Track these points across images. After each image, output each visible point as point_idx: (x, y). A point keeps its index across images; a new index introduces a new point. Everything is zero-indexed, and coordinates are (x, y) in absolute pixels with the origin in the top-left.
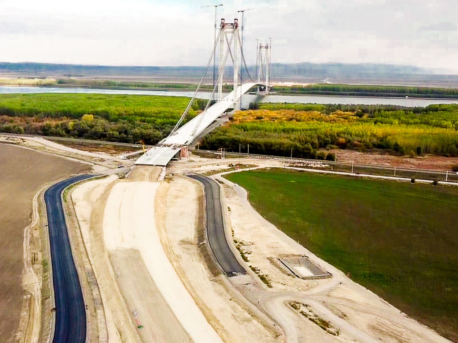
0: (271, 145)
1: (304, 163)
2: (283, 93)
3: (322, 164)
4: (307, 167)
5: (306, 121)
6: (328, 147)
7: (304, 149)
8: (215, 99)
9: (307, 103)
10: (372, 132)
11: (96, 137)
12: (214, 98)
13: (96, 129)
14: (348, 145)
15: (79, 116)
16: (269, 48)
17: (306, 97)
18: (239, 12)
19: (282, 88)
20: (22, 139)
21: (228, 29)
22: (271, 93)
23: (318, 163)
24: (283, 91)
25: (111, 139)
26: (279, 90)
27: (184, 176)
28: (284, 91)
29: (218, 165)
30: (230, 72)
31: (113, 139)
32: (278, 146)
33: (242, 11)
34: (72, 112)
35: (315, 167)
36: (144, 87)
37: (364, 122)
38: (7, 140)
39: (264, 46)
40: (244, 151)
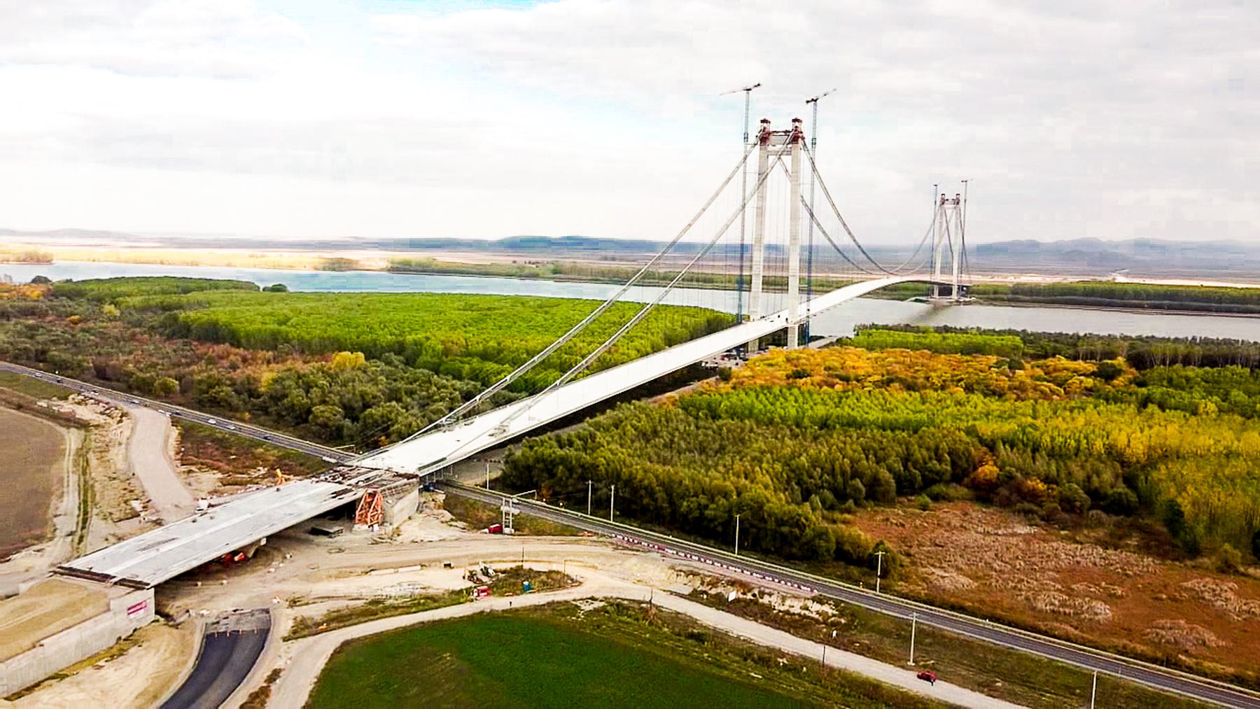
3: (814, 599)
4: (751, 609)
6: (1011, 461)
8: (744, 312)
10: (1111, 441)
16: (962, 202)
18: (808, 102)
19: (992, 290)
21: (776, 145)
26: (984, 293)
28: (996, 296)
32: (703, 500)
33: (813, 100)
37: (1107, 400)
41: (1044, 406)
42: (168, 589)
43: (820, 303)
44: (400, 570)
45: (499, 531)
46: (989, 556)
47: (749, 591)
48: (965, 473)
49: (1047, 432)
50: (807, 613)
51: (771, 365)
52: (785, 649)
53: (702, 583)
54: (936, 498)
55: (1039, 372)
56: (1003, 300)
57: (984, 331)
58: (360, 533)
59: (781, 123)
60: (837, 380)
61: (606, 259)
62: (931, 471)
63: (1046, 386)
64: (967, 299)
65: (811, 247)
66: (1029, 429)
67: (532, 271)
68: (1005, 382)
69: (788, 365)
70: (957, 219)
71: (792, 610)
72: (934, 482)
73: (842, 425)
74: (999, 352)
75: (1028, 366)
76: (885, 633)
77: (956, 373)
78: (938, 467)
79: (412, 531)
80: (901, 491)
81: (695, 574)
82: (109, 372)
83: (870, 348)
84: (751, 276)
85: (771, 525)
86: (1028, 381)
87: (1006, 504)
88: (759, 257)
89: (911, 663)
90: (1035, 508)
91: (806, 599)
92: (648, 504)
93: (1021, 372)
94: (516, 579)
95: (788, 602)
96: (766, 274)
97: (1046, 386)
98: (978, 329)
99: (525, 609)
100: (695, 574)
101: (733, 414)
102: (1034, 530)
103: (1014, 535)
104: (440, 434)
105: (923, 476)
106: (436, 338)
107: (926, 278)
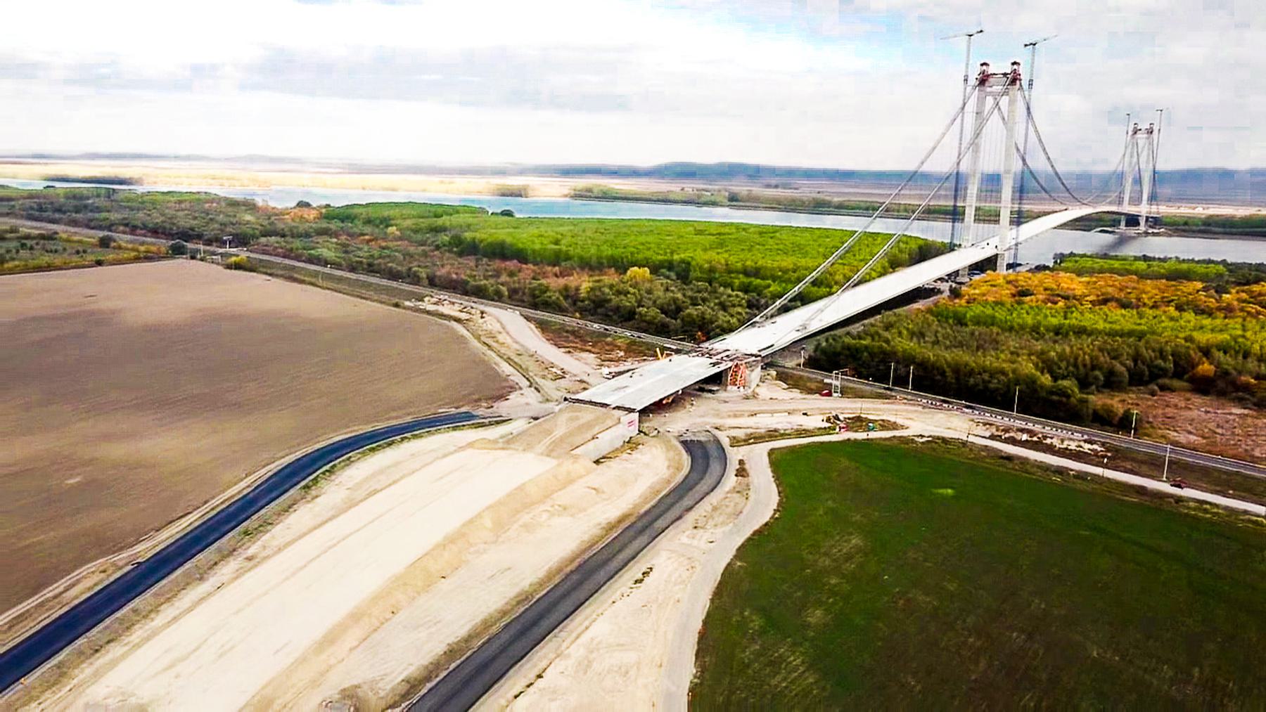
2: (1184, 231)
3: (1085, 441)
7: (1052, 393)
9: (1201, 258)
11: (619, 317)
14: (1221, 384)
16: (1156, 132)
17: (1240, 242)
18: (1026, 45)
20: (482, 313)
21: (996, 87)
22: (1150, 231)
24: (1183, 228)
30: (992, 182)
36: (868, 210)
38: (461, 311)
39: (1143, 129)
41: (1252, 323)
43: (1029, 229)
44: (775, 415)
45: (829, 394)
46: (1212, 426)
47: (1035, 435)
48: (1185, 371)
49: (1257, 341)
50: (1081, 449)
51: (994, 286)
52: (1072, 467)
53: (997, 430)
54: (1163, 388)
55: (1244, 296)
56: (1194, 232)
57: (1184, 260)
58: (732, 392)
59: (1000, 66)
60: (1060, 299)
61: (768, 186)
62: (1156, 366)
63: (1252, 308)
64: (1156, 231)
65: (958, 173)
66: (1240, 340)
67: (708, 199)
68: (1212, 303)
69: (1009, 286)
70: (1149, 149)
71: (1069, 447)
72: (1159, 377)
73: (1074, 333)
74: (1204, 278)
75: (1234, 291)
76: (1143, 462)
77: (1166, 295)
78: (1163, 364)
79: (764, 391)
80: (1131, 384)
81: (991, 425)
83: (1079, 274)
84: (964, 207)
85: (1044, 394)
86: (1235, 303)
87: (1222, 394)
88: (973, 189)
89: (1164, 479)
90: (1247, 396)
91: (1080, 441)
92: (939, 381)
93: (1228, 296)
94: (858, 422)
95: (1066, 443)
97: (1252, 308)
98: (1177, 258)
99: (876, 439)
100: (991, 425)
101: (978, 321)
102: (1246, 412)
103: (1231, 414)
104: (756, 329)
105: (1150, 371)
106: (701, 257)
107: (1114, 208)
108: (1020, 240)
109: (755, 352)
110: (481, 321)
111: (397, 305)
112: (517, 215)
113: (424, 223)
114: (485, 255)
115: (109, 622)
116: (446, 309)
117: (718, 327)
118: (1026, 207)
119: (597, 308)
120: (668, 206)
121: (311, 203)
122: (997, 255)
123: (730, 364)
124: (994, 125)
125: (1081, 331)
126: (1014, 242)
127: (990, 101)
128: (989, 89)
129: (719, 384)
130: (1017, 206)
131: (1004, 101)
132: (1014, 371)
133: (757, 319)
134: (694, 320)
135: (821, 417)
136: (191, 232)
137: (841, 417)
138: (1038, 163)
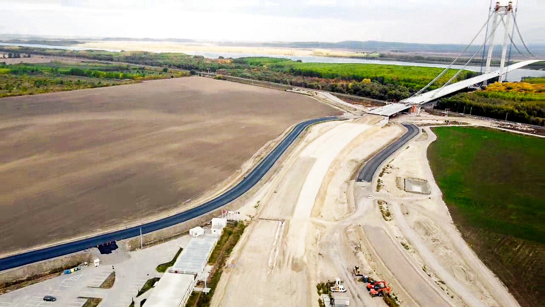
0: (491, 109)
1: (511, 126)
3: (529, 128)
4: (514, 129)
5: (138, 70)
8: (483, 72)
12: (481, 71)
13: (366, 89)
15: (359, 79)
20: (316, 93)
21: (502, 11)
23: (526, 127)
25: (374, 96)
27: (401, 125)
29: (437, 121)
31: (374, 97)
32: (497, 110)
34: (359, 77)
35: (520, 130)
40: (467, 112)
42: (391, 117)
82: (292, 83)
94: (455, 122)
96: (500, 59)
106: (389, 76)
108: (508, 71)
109: (418, 103)
110: (317, 96)
111: (285, 91)
112: (303, 62)
113: (274, 64)
114: (305, 76)
115: (6, 272)
116: (302, 92)
117: (403, 96)
118: (511, 60)
119: (356, 91)
120: (354, 59)
121: (224, 57)
122: (499, 76)
123: (411, 106)
124: (500, 28)
125: (530, 100)
126: (506, 72)
127: (499, 17)
128: (499, 13)
129: (408, 112)
130: (508, 60)
131: (505, 17)
132: (506, 109)
133: (416, 94)
134: (392, 95)
135: (443, 121)
136: (193, 67)
137: (449, 121)
138: (517, 41)
